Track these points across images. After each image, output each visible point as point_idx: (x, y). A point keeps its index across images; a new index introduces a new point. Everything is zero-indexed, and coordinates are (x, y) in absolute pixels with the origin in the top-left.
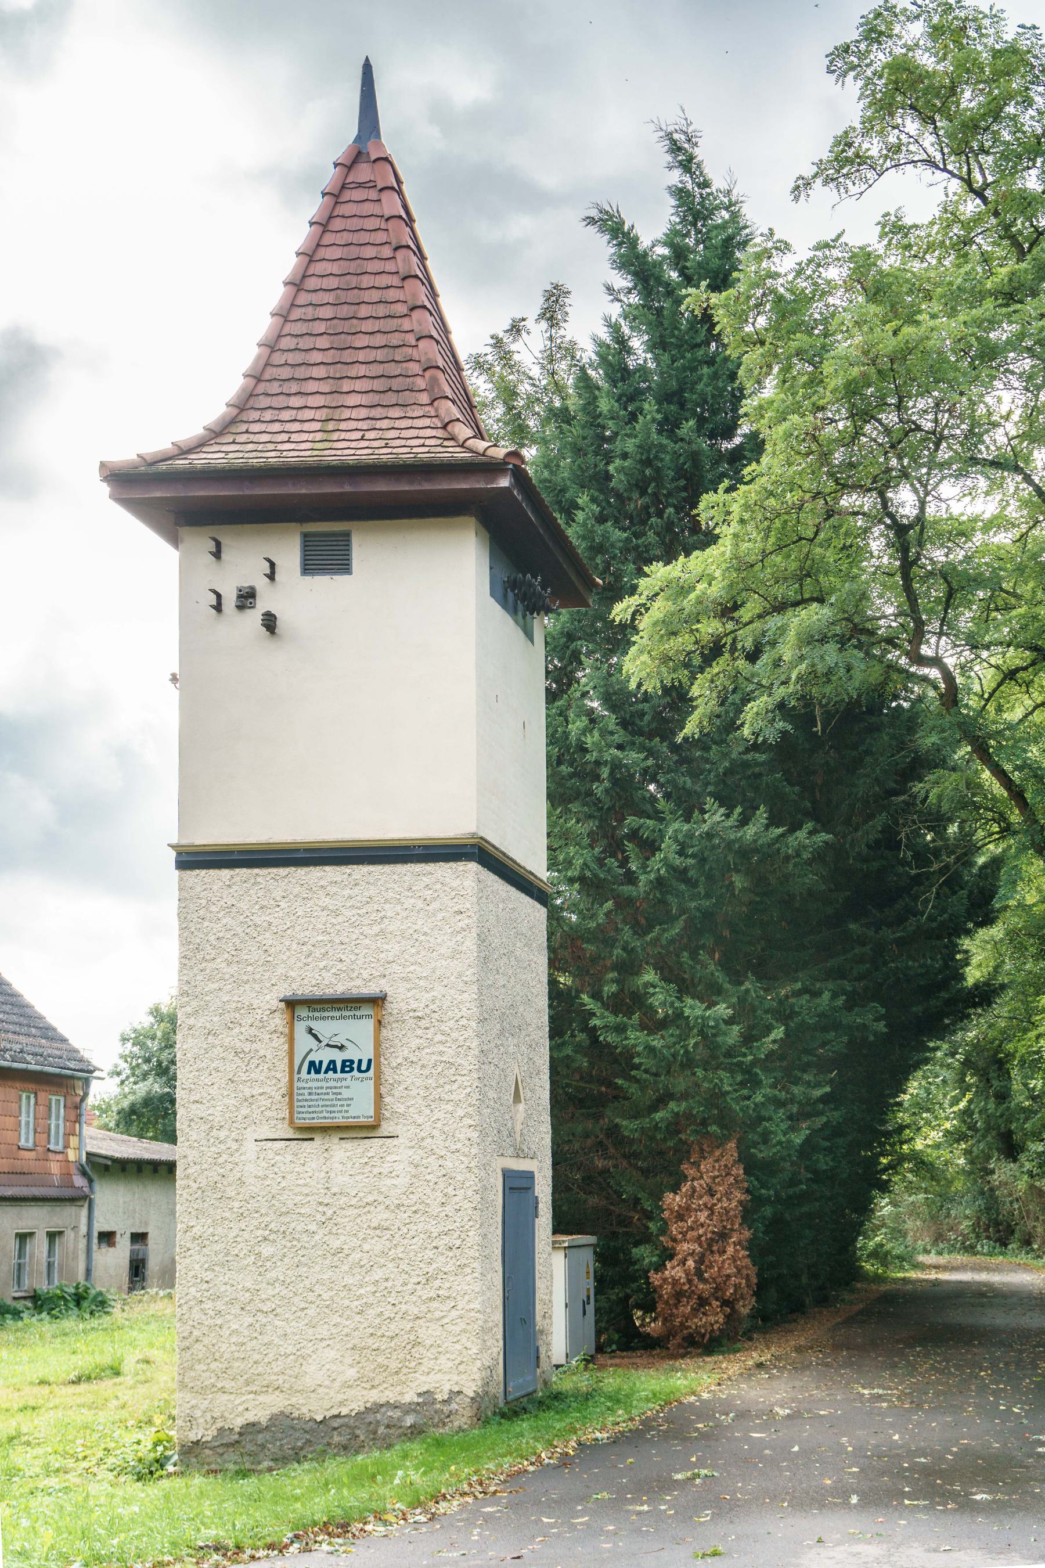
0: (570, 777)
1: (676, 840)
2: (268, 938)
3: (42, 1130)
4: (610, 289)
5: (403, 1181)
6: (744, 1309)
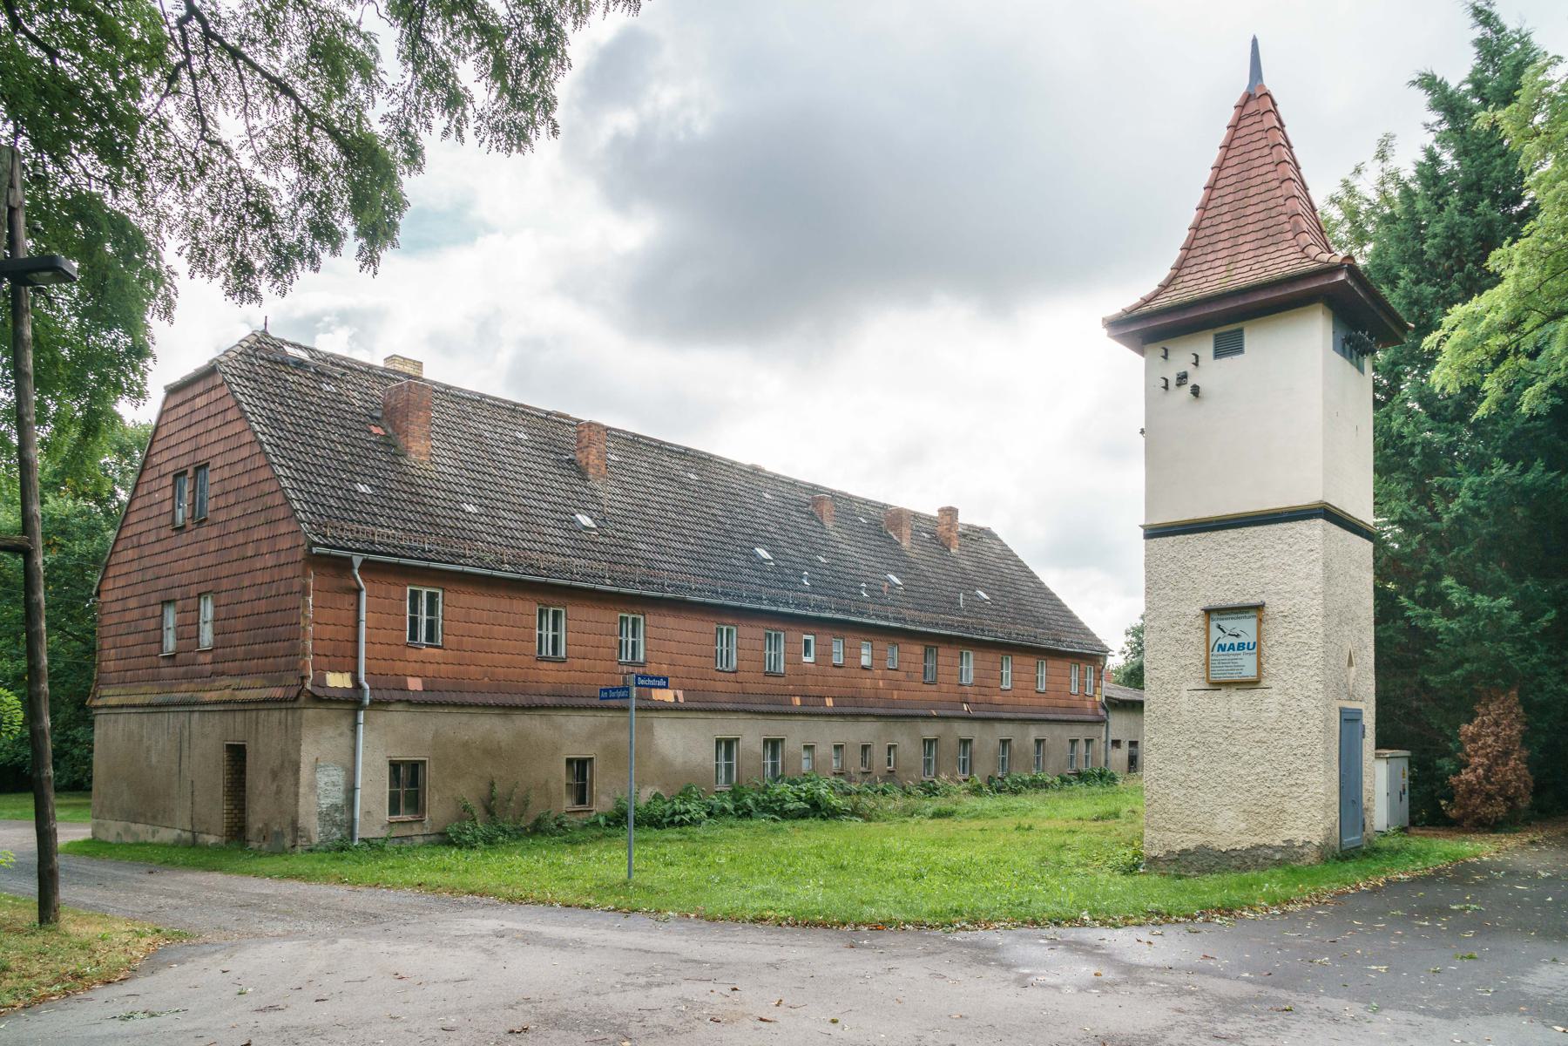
0: (1392, 456)
1: (1470, 489)
2: (1194, 574)
3: (1082, 685)
4: (1426, 126)
5: (1275, 714)
6: (1523, 803)
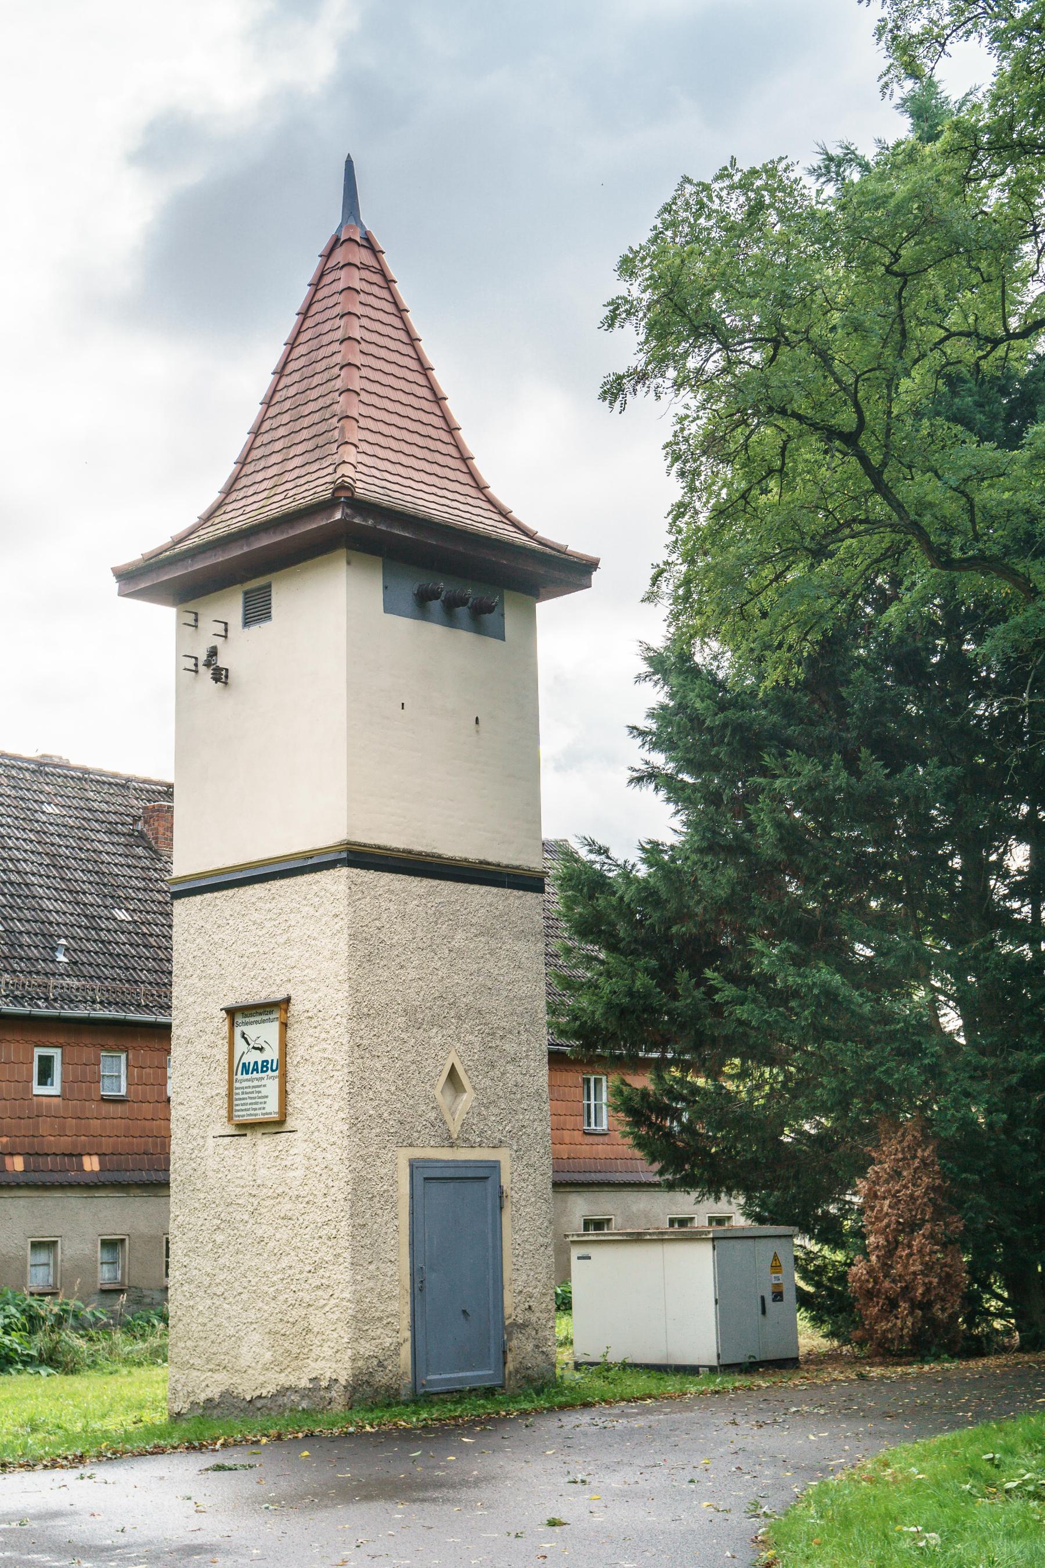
5: (300, 1173)
